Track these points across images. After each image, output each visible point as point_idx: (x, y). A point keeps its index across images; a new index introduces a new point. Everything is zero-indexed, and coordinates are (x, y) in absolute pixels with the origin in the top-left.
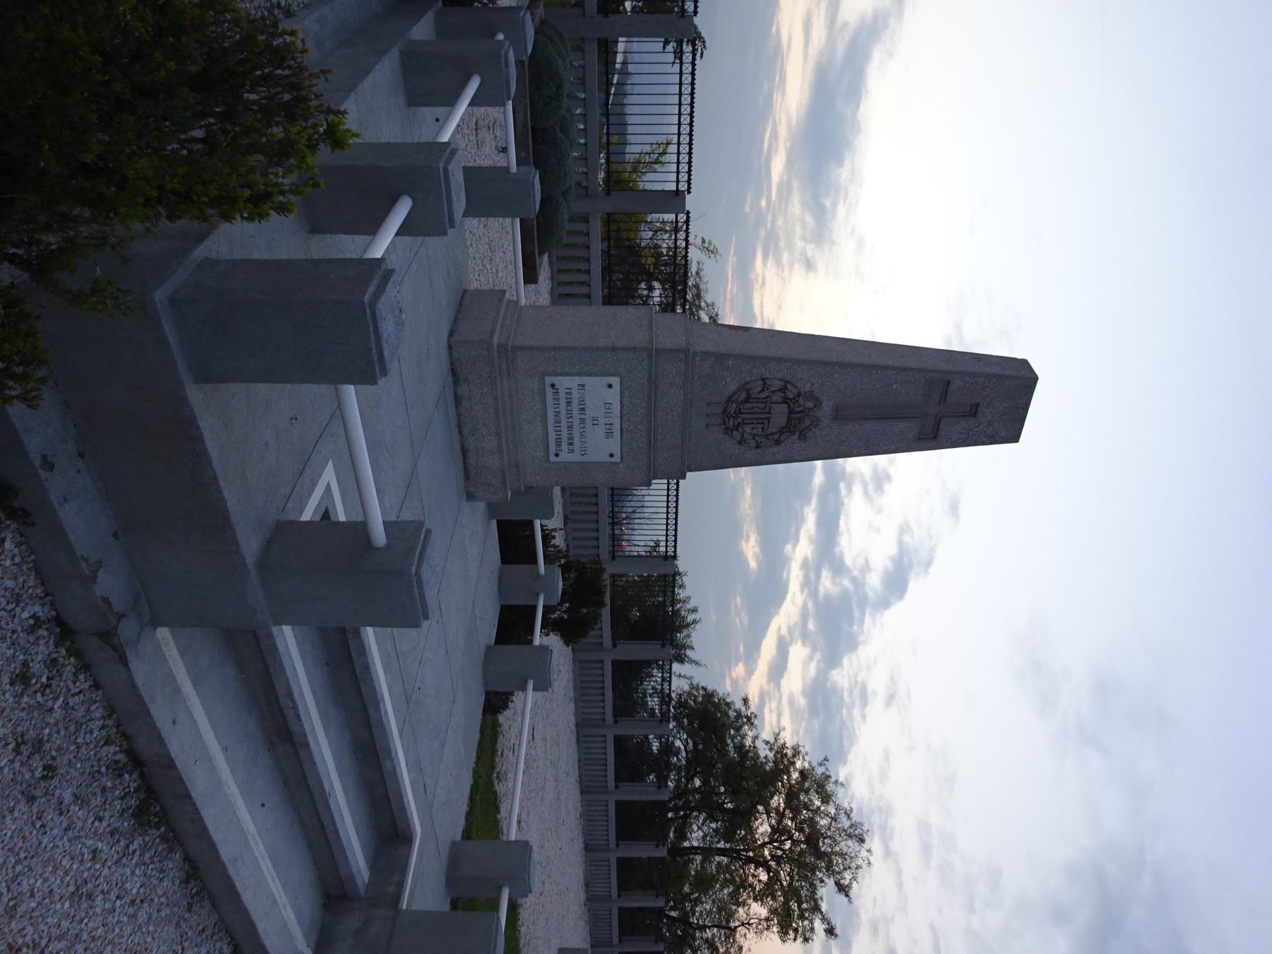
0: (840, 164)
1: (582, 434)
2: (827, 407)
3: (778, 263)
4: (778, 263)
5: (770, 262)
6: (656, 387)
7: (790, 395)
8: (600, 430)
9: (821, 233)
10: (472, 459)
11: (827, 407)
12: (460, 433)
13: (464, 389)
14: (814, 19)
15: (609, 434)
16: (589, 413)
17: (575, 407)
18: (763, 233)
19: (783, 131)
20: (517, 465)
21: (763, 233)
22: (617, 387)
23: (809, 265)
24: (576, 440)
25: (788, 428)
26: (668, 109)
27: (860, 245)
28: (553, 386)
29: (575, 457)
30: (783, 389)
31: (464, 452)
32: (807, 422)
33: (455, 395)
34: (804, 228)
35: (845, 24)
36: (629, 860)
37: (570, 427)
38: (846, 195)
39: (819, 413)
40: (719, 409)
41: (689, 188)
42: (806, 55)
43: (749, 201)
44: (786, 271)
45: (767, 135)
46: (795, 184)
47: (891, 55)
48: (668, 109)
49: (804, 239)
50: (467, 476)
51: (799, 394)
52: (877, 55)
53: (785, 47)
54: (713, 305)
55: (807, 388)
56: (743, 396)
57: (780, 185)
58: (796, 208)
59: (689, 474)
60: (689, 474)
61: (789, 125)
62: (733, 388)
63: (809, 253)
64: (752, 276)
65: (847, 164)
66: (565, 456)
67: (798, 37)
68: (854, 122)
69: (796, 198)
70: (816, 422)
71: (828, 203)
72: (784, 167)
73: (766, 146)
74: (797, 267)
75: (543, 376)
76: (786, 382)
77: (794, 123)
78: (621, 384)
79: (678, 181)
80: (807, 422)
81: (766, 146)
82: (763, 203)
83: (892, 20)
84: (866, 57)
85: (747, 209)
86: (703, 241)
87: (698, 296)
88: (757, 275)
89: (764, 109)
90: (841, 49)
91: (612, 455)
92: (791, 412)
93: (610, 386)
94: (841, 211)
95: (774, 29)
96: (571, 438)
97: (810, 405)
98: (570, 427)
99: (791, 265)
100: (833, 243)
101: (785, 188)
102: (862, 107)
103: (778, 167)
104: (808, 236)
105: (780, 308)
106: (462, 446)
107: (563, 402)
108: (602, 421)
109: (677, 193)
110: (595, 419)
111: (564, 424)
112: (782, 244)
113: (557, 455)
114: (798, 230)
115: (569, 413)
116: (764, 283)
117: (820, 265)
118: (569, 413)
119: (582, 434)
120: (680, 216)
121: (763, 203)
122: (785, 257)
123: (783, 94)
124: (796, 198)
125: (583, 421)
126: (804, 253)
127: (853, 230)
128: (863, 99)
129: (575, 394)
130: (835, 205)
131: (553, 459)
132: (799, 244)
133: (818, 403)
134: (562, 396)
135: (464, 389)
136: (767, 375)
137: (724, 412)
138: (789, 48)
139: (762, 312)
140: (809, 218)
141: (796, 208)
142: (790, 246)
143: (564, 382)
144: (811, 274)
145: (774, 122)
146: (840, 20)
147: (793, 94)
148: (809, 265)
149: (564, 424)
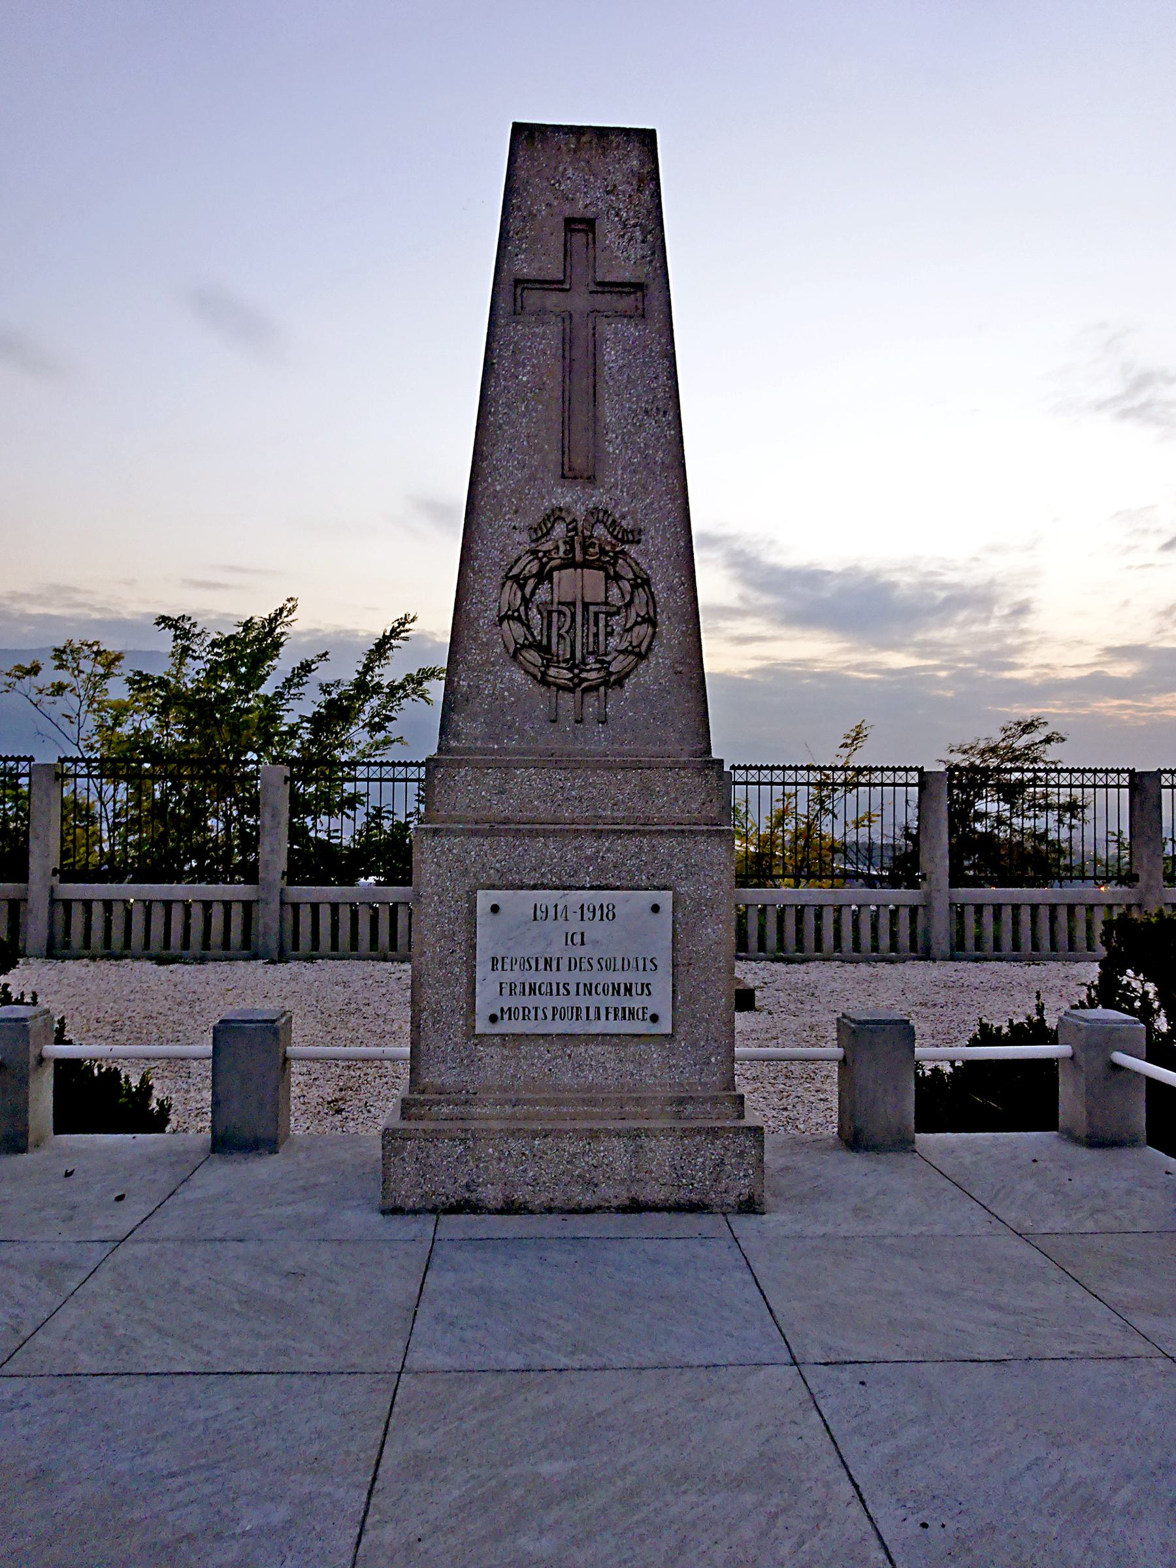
0: (894, 585)
1: (607, 965)
2: (564, 496)
3: (1018, 650)
4: (1018, 650)
5: (1019, 660)
6: (506, 821)
7: (534, 567)
8: (596, 930)
9: (974, 600)
10: (654, 1193)
11: (564, 496)
12: (589, 1210)
13: (491, 1194)
14: (736, 633)
15: (607, 913)
16: (557, 949)
17: (540, 977)
18: (982, 672)
19: (856, 658)
20: (681, 1101)
21: (982, 672)
22: (495, 896)
23: (1022, 610)
24: (621, 978)
25: (606, 563)
26: (888, 799)
27: (994, 549)
28: (493, 1019)
29: (662, 983)
30: (520, 581)
31: (636, 1207)
32: (600, 531)
33: (499, 1212)
34: (973, 621)
35: (742, 598)
36: (76, 1063)
37: (589, 989)
38: (932, 573)
39: (580, 511)
40: (568, 701)
41: (25, 759)
42: (774, 639)
43: (941, 692)
44: (1031, 638)
45: (862, 675)
46: (919, 637)
47: (772, 543)
48: (888, 799)
49: (987, 620)
50: (697, 1208)
51: (534, 552)
52: (772, 558)
53: (765, 662)
54: (1005, 730)
55: (524, 537)
56: (532, 656)
57: (921, 655)
58: (949, 634)
59: (715, 755)
60: (715, 755)
61: (850, 650)
62: (519, 676)
63: (1006, 611)
64: (1037, 682)
65: (894, 577)
66: (660, 1001)
67: (754, 649)
68: (851, 573)
69: (936, 635)
70: (597, 515)
71: (942, 595)
72: (899, 651)
73: (875, 676)
74: (1024, 626)
75: (471, 1033)
76: (507, 578)
77: (848, 645)
78: (493, 887)
79: (907, 785)
80: (600, 531)
81: (875, 676)
82: (943, 674)
83: (736, 546)
84: (774, 569)
85: (950, 694)
86: (845, 745)
87: (993, 750)
88: (1037, 675)
89: (832, 679)
90: (766, 600)
91: (655, 909)
92: (569, 563)
93: (495, 909)
94: (951, 577)
95: (746, 676)
96: (616, 990)
97: (560, 529)
98: (589, 989)
99: (1023, 632)
100: (991, 583)
101: (924, 649)
102: (828, 568)
103: (898, 660)
104: (983, 615)
105: (1080, 642)
106: (623, 1210)
107: (531, 1001)
108: (575, 925)
109: (1132, 787)
110: (569, 939)
111: (583, 1001)
112: (994, 647)
113: (654, 1018)
114: (975, 628)
115: (555, 989)
116: (1047, 666)
117: (1020, 597)
118: (555, 989)
119: (607, 965)
120: (1164, 782)
121: (943, 674)
122: (1012, 641)
123: (816, 661)
124: (936, 635)
125: (575, 964)
126: (1005, 618)
127: (976, 559)
128: (818, 568)
129: (514, 976)
130: (944, 586)
131: (665, 1027)
132: (993, 626)
133: (555, 515)
134: (517, 1002)
135: (491, 1194)
136: (492, 615)
137: (571, 690)
138: (766, 658)
139: (1087, 665)
140: (961, 617)
141: (949, 634)
142: (998, 636)
143: (487, 998)
144: (1034, 606)
145: (848, 668)
146: (738, 604)
147: (815, 649)
148: (1022, 610)
149: (583, 1001)
